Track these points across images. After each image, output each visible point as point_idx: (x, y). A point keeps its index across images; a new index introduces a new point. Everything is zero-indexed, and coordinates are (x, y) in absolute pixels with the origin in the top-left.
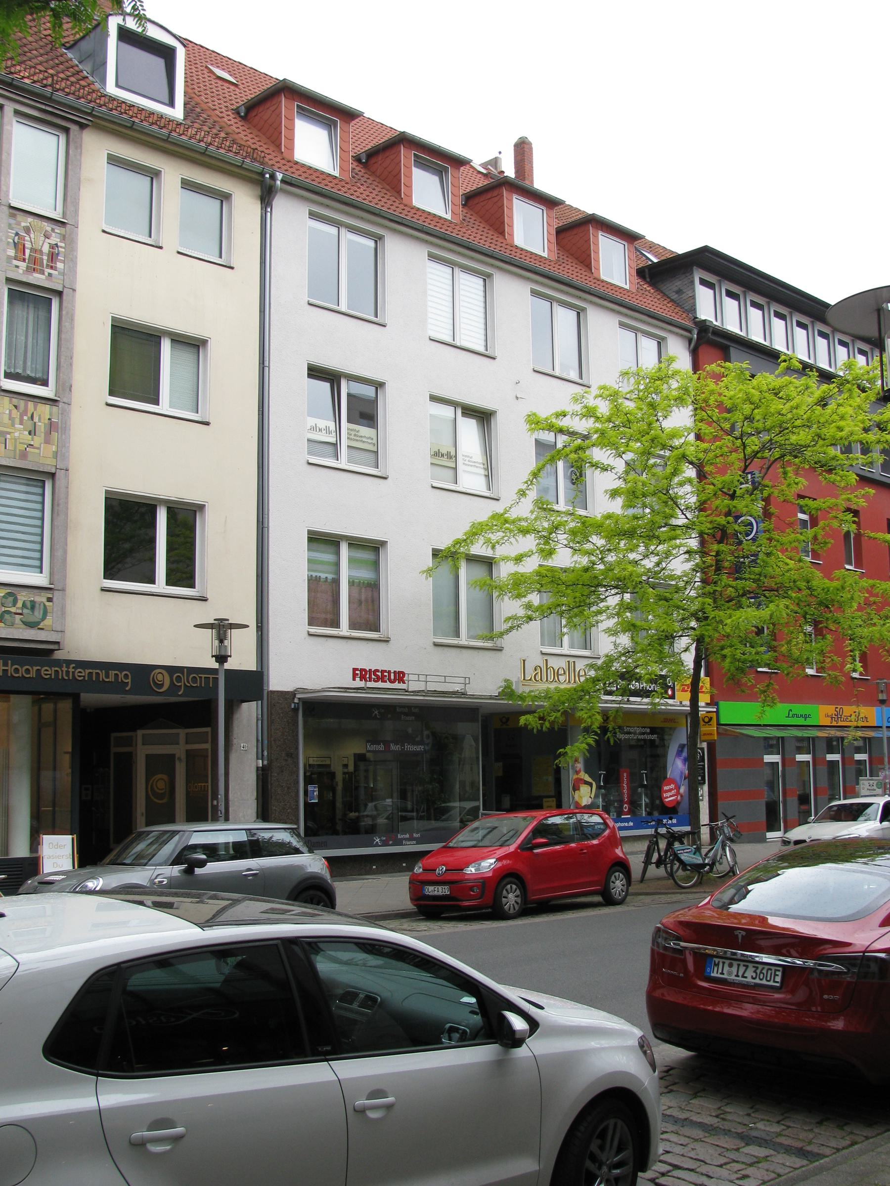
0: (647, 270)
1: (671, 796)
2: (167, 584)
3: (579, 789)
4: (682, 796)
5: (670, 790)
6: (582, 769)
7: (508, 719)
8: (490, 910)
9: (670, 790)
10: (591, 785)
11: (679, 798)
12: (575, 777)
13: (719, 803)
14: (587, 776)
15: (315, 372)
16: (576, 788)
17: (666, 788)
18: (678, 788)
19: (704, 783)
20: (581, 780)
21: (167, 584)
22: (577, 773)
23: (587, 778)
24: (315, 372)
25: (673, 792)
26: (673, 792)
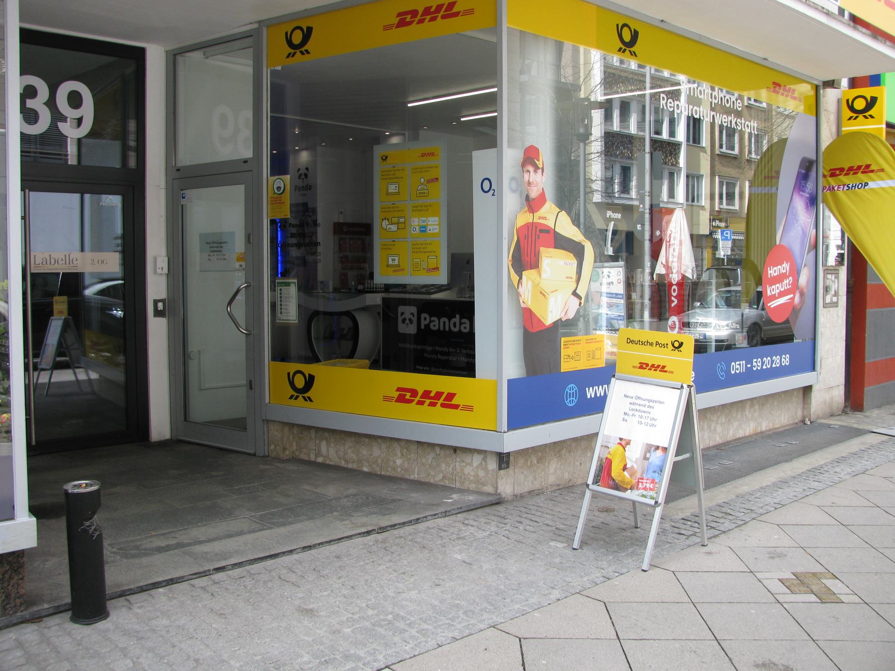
0: (493, 39)
1: (782, 294)
2: (509, 381)
3: (535, 264)
4: (802, 294)
5: (780, 279)
6: (549, 194)
7: (307, 34)
8: (267, 401)
9: (780, 279)
10: (577, 251)
11: (797, 299)
12: (525, 218)
13: (870, 312)
14: (564, 218)
15: (288, 57)
16: (524, 259)
17: (773, 272)
18: (795, 273)
19: (843, 265)
20: (546, 230)
21: (509, 381)
22: (532, 204)
23: (566, 228)
24: (288, 57)
25: (787, 283)
26: (787, 283)
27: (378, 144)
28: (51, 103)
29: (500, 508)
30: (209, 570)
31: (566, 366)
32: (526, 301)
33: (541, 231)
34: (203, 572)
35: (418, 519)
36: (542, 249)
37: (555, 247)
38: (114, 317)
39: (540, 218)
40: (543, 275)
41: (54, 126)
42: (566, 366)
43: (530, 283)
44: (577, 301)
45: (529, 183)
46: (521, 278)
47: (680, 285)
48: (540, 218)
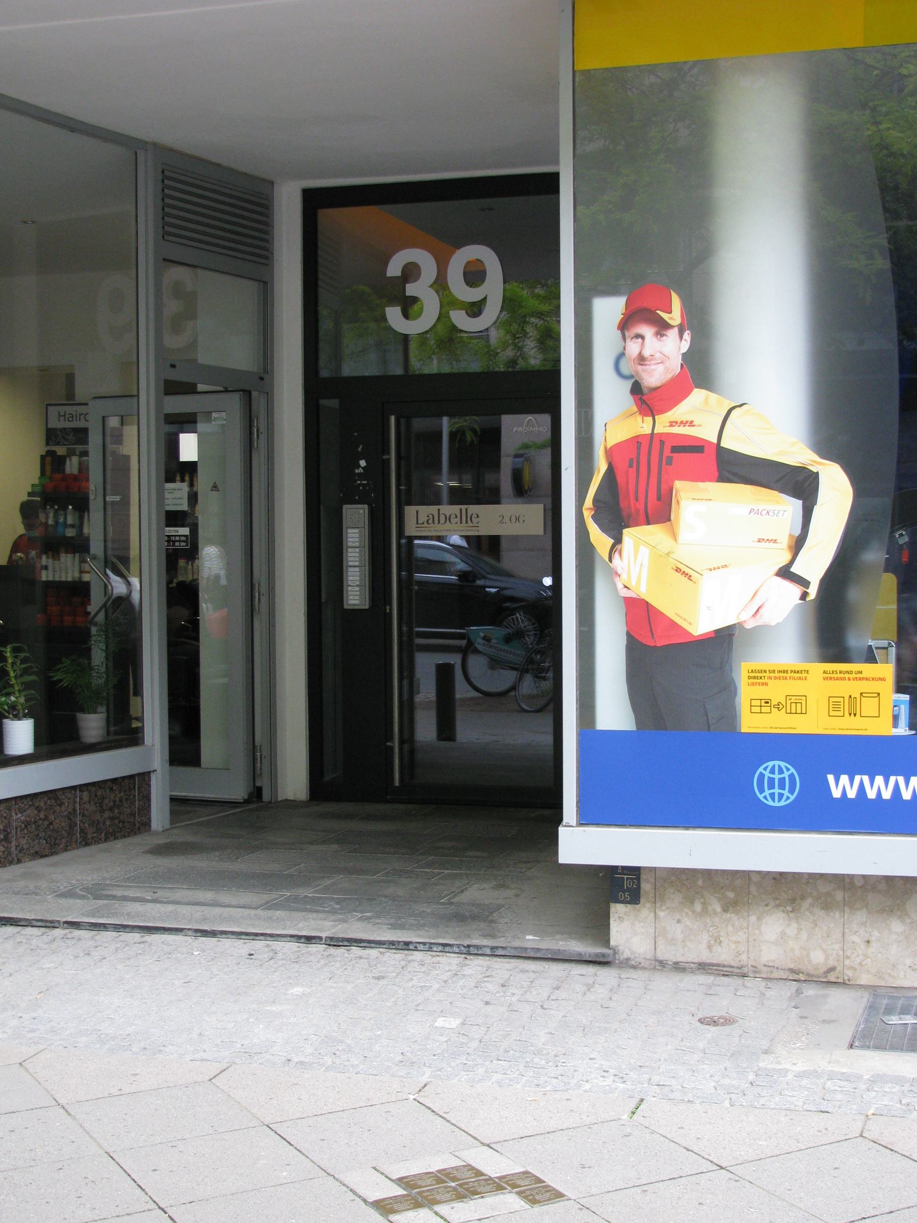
3: (660, 512)
27: (197, 360)
28: (440, 284)
29: (603, 973)
30: (58, 922)
31: (751, 722)
32: (632, 584)
33: (676, 449)
34: (52, 922)
35: (407, 944)
36: (678, 484)
37: (722, 479)
38: (490, 593)
39: (672, 424)
40: (684, 534)
41: (443, 317)
42: (751, 722)
43: (644, 552)
44: (795, 591)
45: (641, 359)
46: (618, 540)
47: (208, 578)
48: (672, 424)
